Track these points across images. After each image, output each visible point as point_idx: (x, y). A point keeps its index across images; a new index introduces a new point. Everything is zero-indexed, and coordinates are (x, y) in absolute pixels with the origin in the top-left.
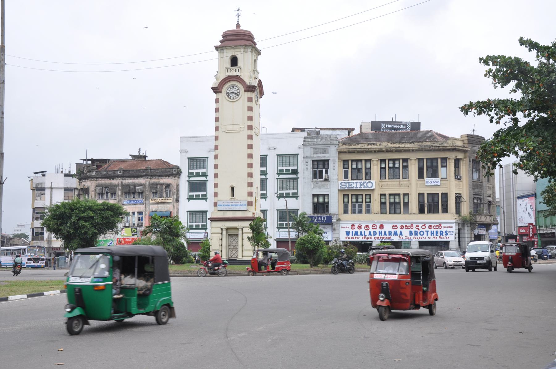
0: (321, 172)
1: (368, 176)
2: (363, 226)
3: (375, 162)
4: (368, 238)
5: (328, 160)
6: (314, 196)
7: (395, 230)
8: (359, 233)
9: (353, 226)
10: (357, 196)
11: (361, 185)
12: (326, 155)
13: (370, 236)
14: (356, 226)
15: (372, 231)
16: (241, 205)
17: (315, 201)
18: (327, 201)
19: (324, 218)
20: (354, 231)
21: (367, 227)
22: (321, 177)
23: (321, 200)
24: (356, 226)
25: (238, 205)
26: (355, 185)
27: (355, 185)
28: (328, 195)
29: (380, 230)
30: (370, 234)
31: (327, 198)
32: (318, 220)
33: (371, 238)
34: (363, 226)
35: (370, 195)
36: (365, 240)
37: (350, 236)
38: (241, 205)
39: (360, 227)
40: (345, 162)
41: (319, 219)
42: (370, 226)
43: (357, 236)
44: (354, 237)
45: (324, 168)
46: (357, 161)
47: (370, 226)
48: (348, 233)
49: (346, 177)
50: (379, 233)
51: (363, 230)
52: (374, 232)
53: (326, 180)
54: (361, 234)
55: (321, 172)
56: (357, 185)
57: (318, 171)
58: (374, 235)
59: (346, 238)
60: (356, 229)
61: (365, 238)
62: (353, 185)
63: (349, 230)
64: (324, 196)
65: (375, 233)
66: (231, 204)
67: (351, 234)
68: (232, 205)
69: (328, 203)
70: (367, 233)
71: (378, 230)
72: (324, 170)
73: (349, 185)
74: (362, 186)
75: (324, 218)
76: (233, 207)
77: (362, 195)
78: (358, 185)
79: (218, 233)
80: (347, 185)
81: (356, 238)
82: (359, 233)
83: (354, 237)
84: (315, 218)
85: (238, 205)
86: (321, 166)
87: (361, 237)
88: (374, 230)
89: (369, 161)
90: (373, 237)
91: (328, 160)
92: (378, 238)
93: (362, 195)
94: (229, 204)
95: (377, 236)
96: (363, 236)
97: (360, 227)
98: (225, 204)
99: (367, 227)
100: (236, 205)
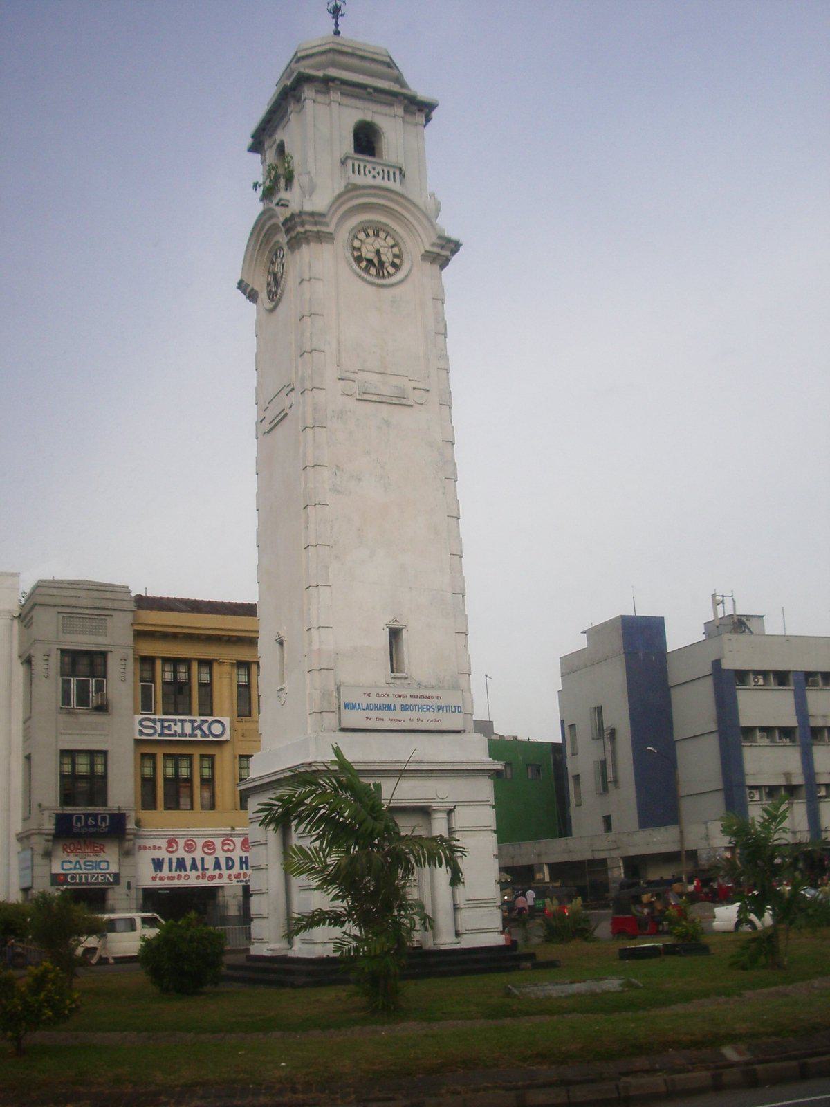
0: (83, 688)
1: (207, 708)
2: (200, 842)
3: (226, 668)
4: (212, 878)
5: (104, 655)
6: (64, 753)
7: (229, 854)
8: (188, 864)
9: (172, 842)
10: (176, 758)
11: (194, 729)
12: (101, 640)
13: (217, 872)
14: (181, 842)
15: (222, 856)
16: (440, 708)
17: (67, 769)
18: (99, 769)
19: (104, 819)
20: (174, 857)
21: (209, 845)
22: (83, 700)
23: (83, 768)
24: (181, 842)
25: (429, 708)
26: (178, 728)
27: (178, 728)
28: (104, 753)
29: (244, 854)
30: (217, 865)
31: (99, 760)
32: (87, 825)
33: (220, 876)
34: (200, 842)
35: (212, 757)
36: (205, 883)
37: (165, 872)
38: (440, 708)
39: (190, 847)
40: (146, 662)
41: (90, 821)
42: (218, 842)
43: (183, 873)
44: (174, 874)
45: (93, 675)
46: (175, 662)
47: (218, 842)
48: (158, 864)
49: (147, 706)
50: (242, 862)
51: (198, 854)
52: (228, 859)
53: (102, 708)
54: (194, 866)
55: (83, 688)
56: (182, 727)
57: (74, 681)
58: (229, 868)
59: (154, 878)
60: (181, 853)
61: (204, 876)
62: (174, 728)
63: (162, 854)
64: (91, 754)
65: (230, 863)
66: (399, 702)
67: (166, 866)
68: (404, 708)
69: (104, 777)
70: (210, 863)
71: (237, 854)
72: (92, 682)
73: (163, 727)
74: (198, 732)
75: (104, 819)
76: (406, 715)
77: (190, 757)
78: (188, 728)
79: (482, 804)
80: (158, 727)
81: (179, 877)
82: (188, 864)
83: (174, 874)
84: (79, 819)
85: (429, 708)
86: (83, 665)
87: (193, 874)
88: (229, 854)
89: (207, 663)
90: (225, 873)
91: (104, 655)
92: (237, 876)
93: (190, 757)
94: (389, 701)
95: (236, 870)
96: (200, 873)
97: (190, 847)
98: (374, 700)
99: (209, 845)
100: (421, 708)
